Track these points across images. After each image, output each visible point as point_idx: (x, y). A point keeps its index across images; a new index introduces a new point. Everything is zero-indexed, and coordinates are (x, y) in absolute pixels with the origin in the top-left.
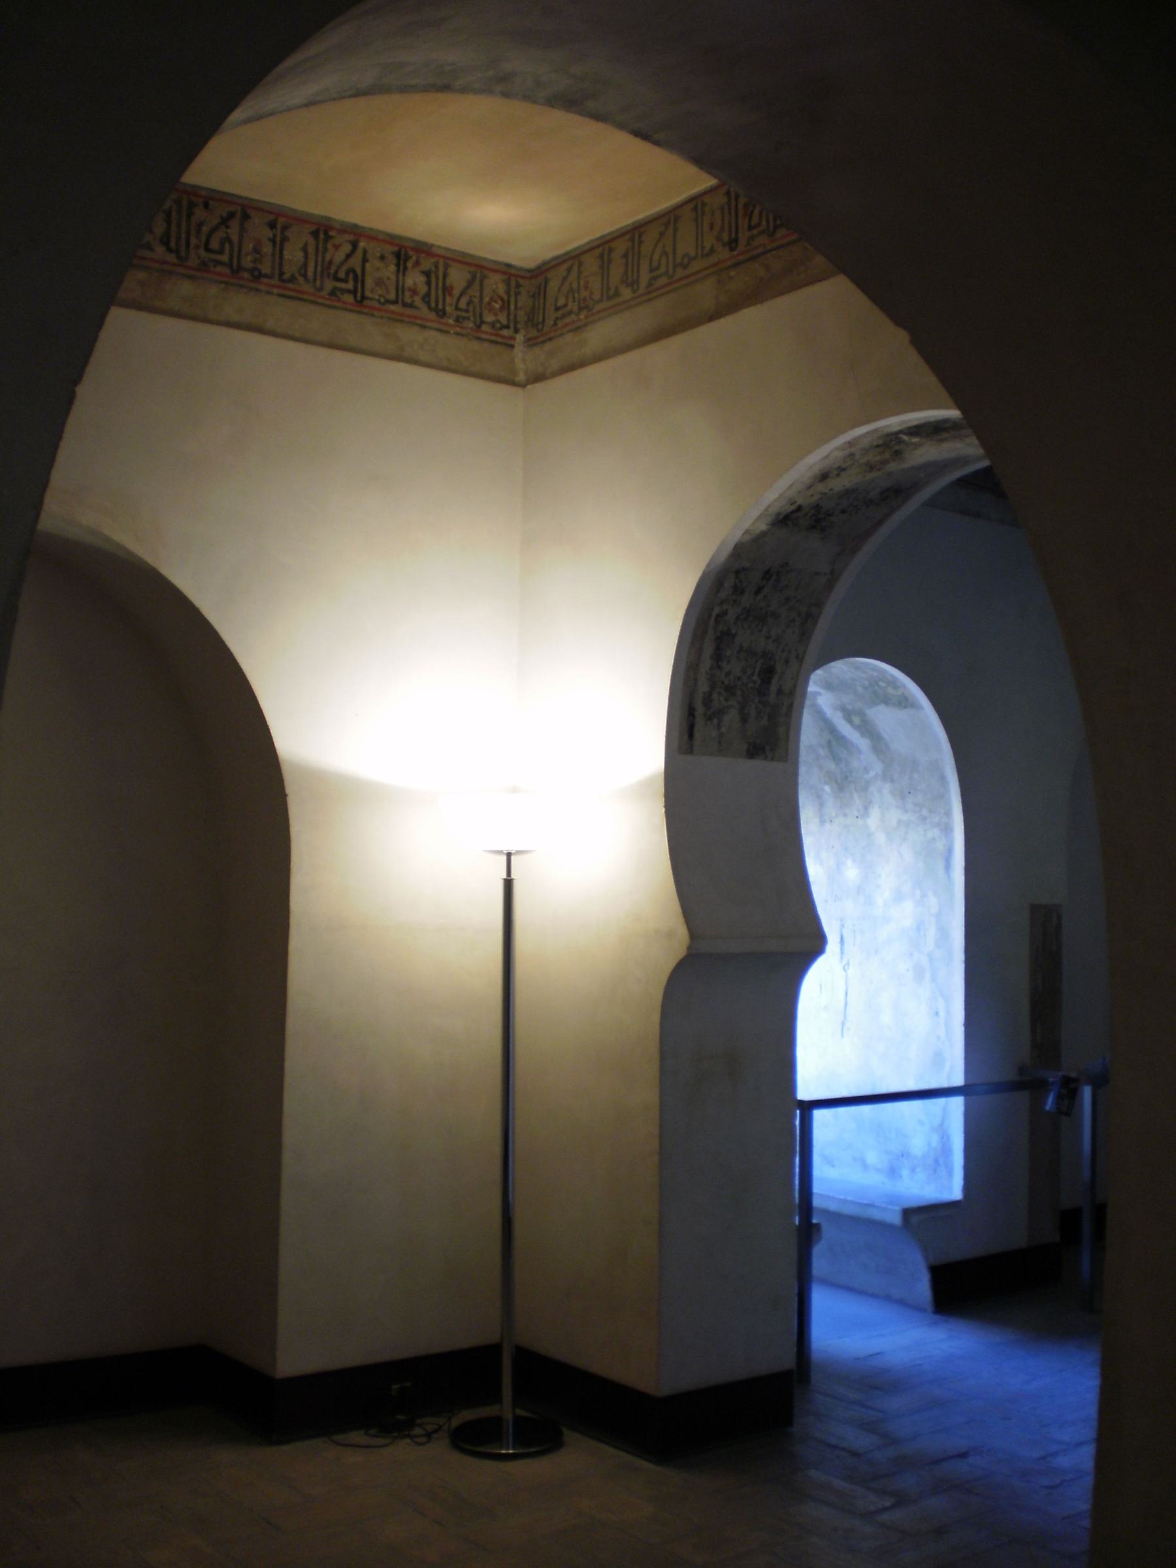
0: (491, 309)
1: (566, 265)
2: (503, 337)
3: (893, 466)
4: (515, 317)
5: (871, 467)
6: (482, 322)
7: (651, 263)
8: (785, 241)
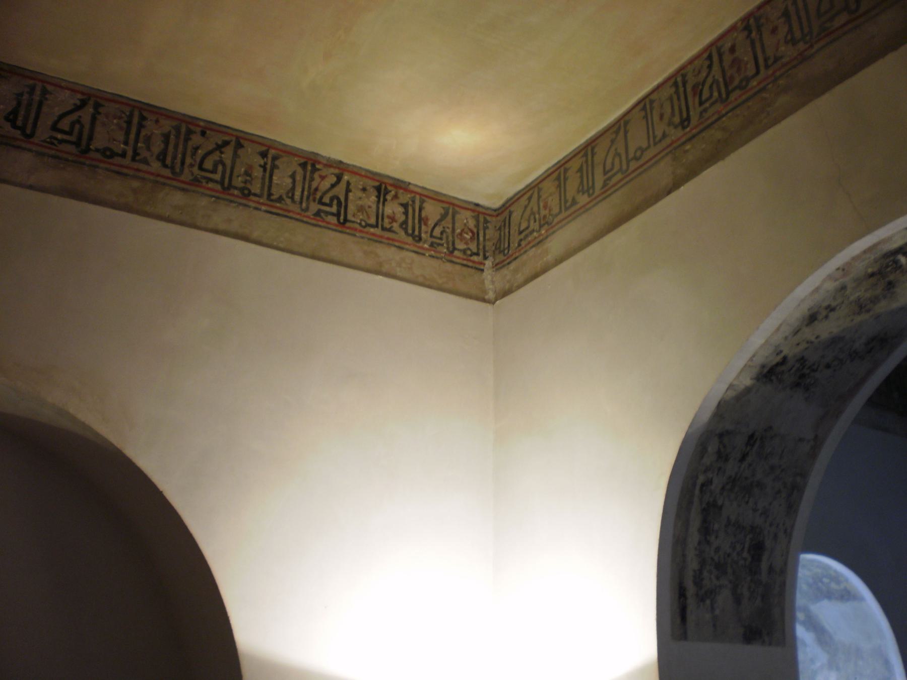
0: (462, 239)
1: (526, 197)
2: (474, 262)
3: (883, 307)
4: (484, 247)
5: (861, 307)
6: (454, 249)
7: (604, 168)
8: (740, 101)
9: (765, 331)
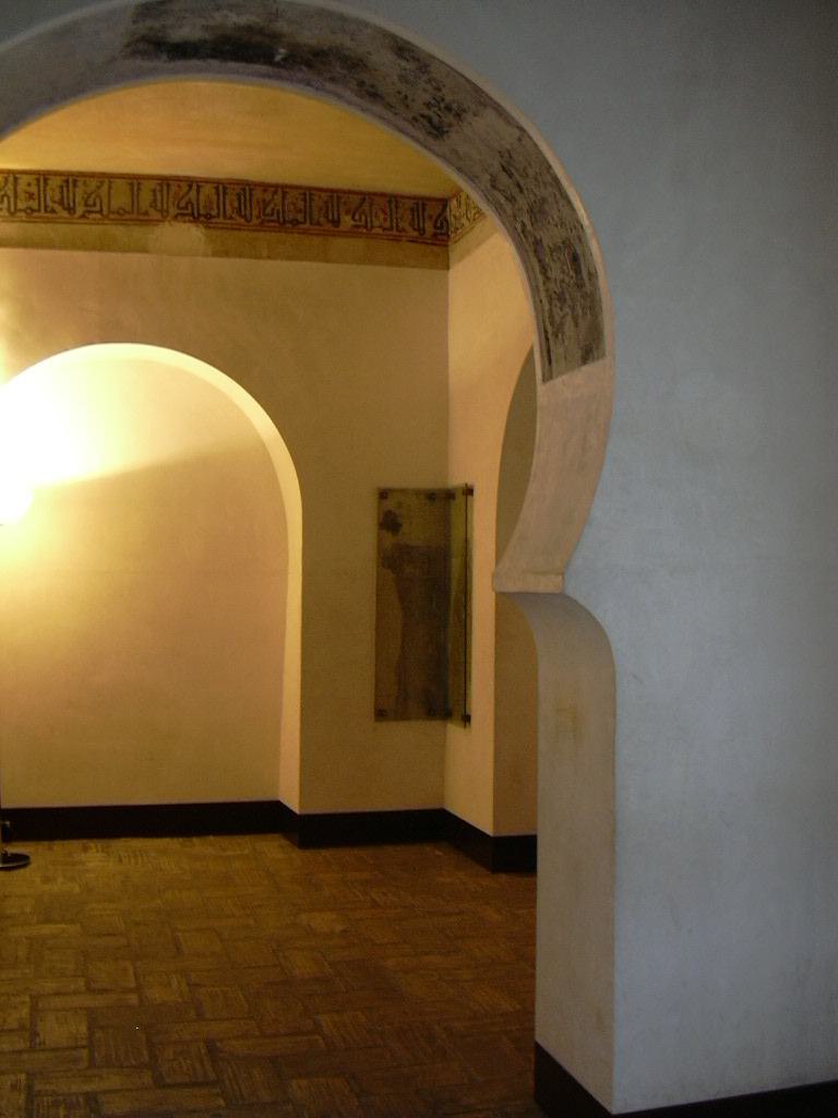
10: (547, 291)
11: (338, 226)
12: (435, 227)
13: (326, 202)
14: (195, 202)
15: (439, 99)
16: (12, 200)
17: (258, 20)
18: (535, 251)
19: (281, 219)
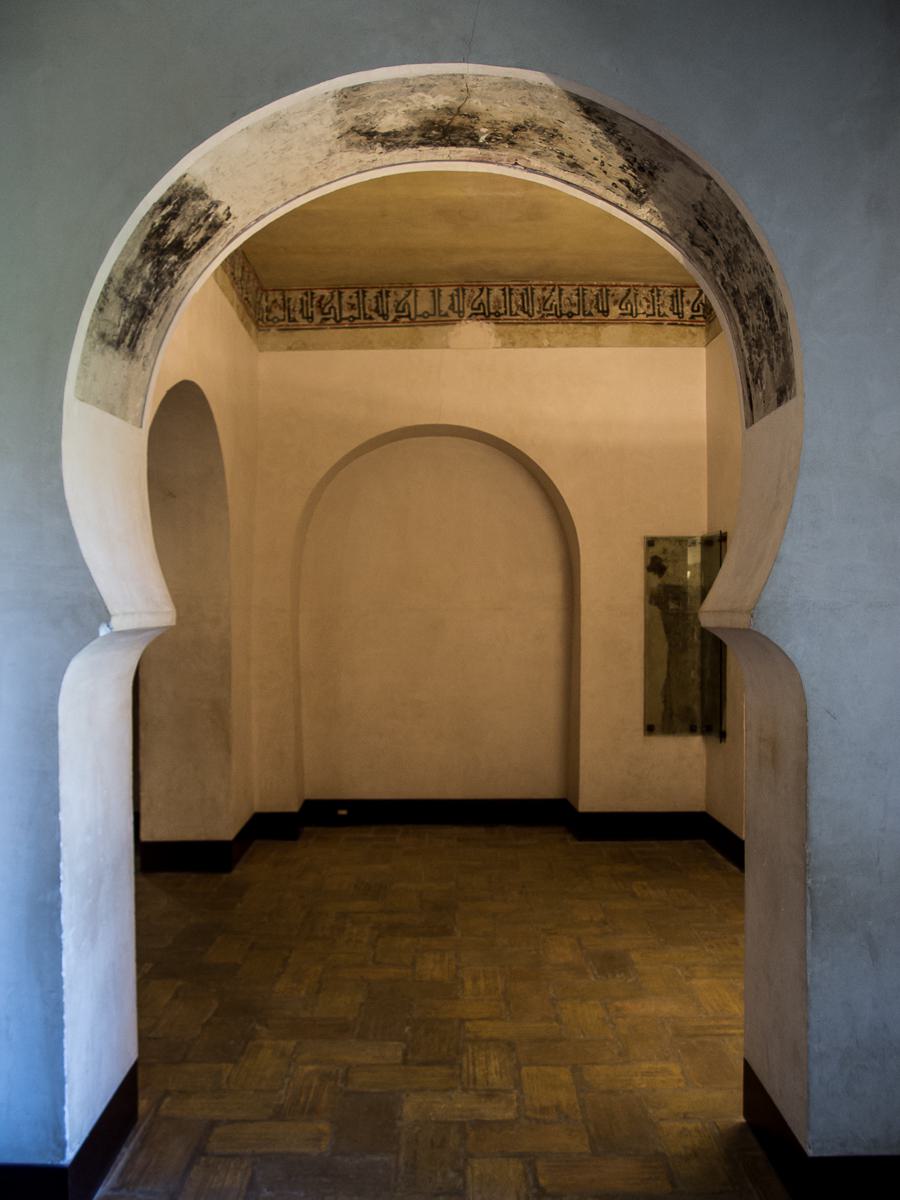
9: (143, 648)
10: (746, 339)
11: (607, 316)
12: (693, 310)
13: (597, 296)
14: (485, 303)
15: (631, 160)
16: (338, 311)
17: (453, 100)
18: (735, 302)
19: (558, 314)
